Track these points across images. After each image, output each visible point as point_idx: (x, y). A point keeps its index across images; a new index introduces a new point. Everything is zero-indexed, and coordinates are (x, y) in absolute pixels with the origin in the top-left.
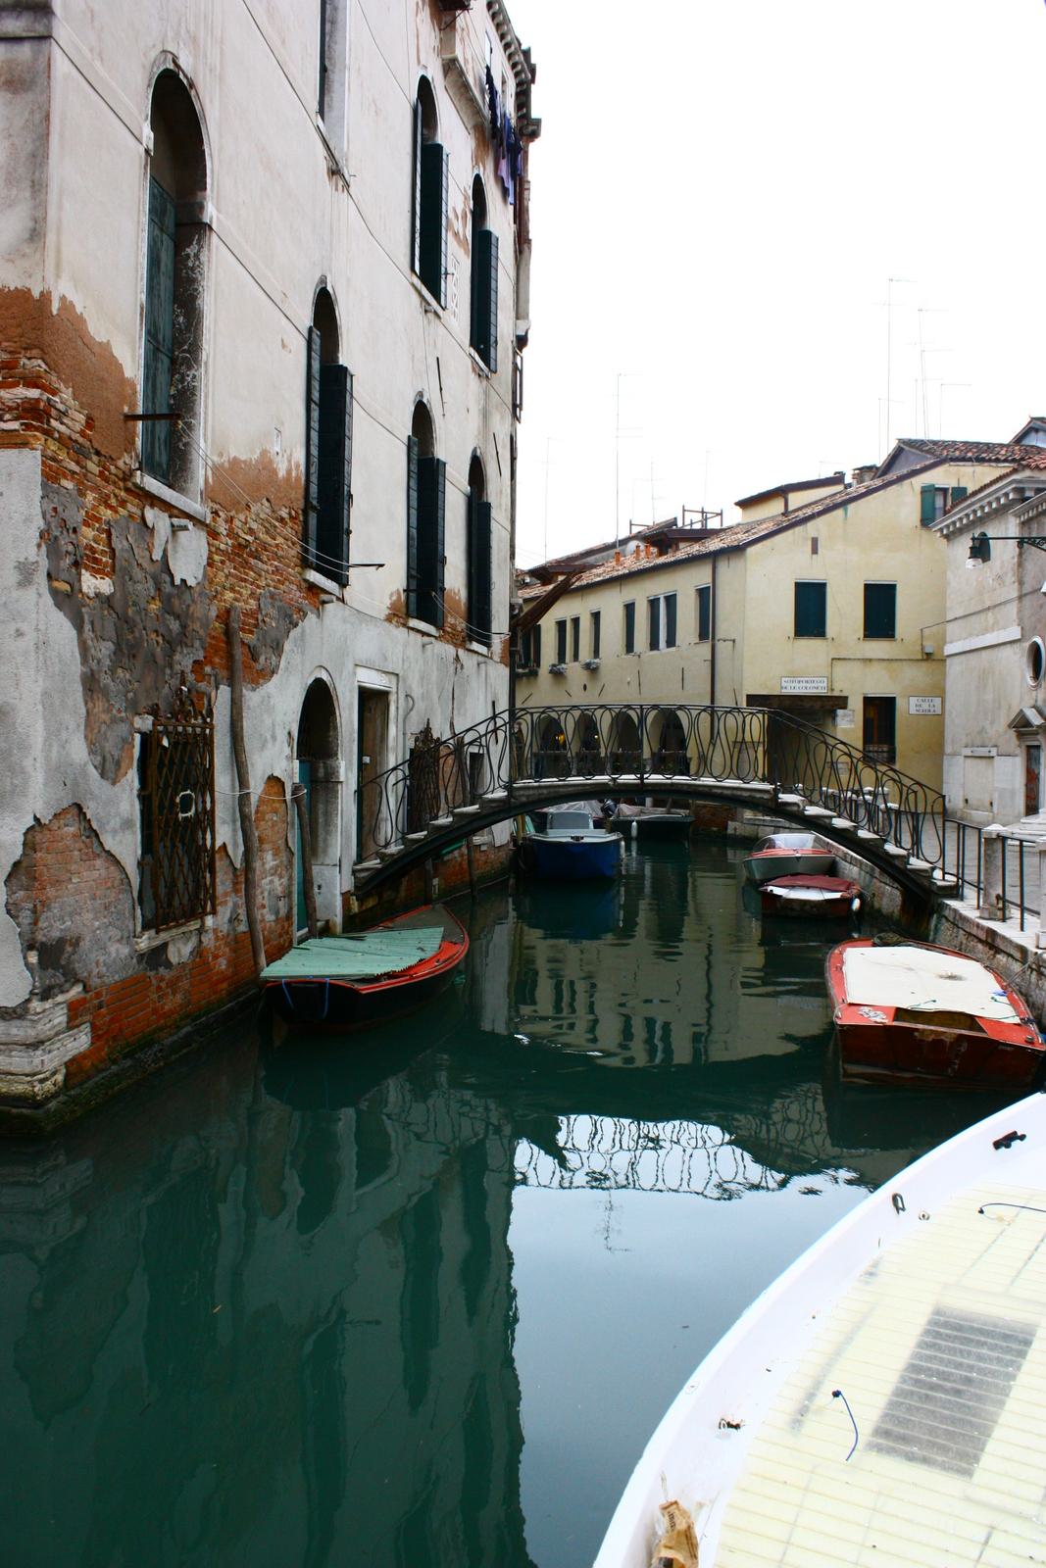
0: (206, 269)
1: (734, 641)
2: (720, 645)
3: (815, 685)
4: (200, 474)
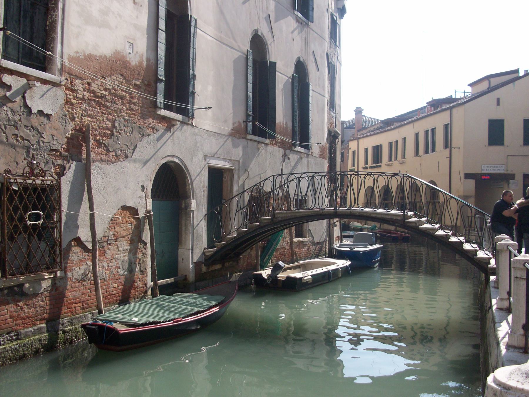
2: (453, 150)
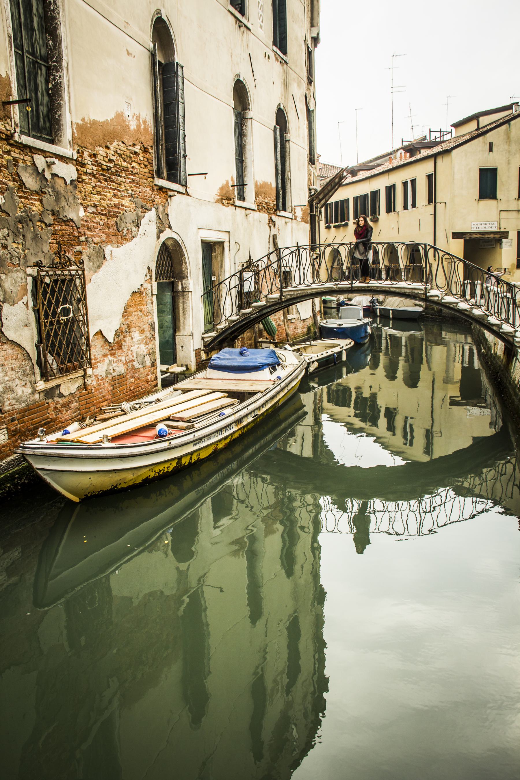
0: (61, 10)
1: (445, 203)
2: (438, 205)
3: (491, 226)
4: (67, 133)
